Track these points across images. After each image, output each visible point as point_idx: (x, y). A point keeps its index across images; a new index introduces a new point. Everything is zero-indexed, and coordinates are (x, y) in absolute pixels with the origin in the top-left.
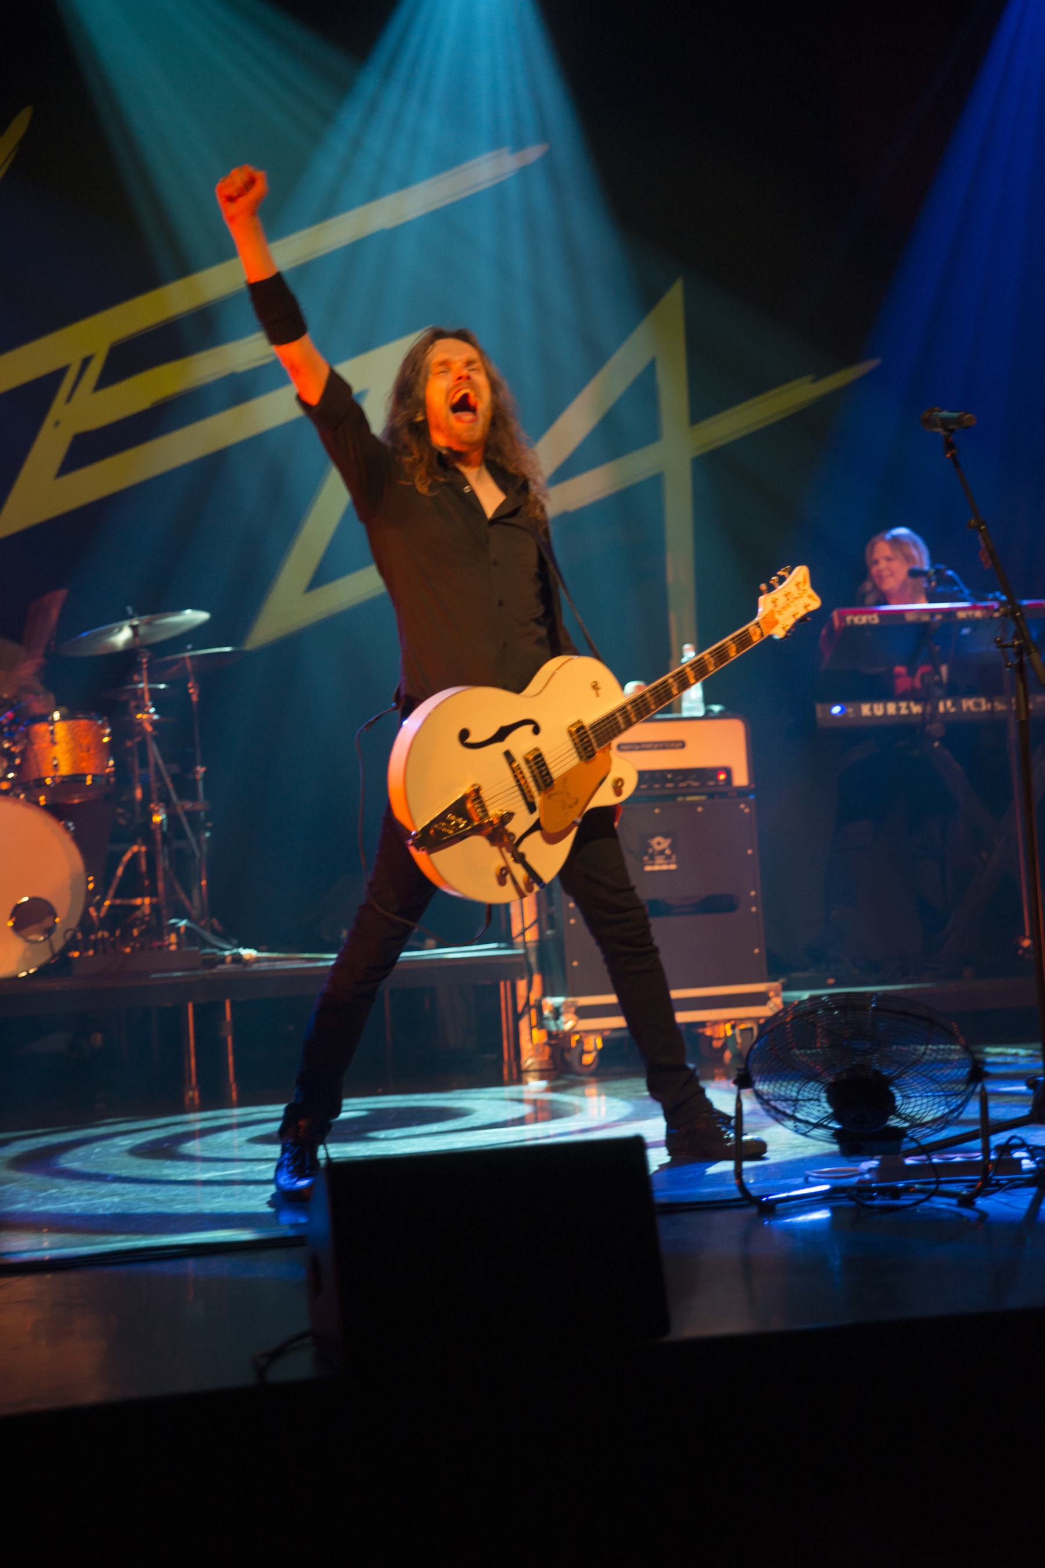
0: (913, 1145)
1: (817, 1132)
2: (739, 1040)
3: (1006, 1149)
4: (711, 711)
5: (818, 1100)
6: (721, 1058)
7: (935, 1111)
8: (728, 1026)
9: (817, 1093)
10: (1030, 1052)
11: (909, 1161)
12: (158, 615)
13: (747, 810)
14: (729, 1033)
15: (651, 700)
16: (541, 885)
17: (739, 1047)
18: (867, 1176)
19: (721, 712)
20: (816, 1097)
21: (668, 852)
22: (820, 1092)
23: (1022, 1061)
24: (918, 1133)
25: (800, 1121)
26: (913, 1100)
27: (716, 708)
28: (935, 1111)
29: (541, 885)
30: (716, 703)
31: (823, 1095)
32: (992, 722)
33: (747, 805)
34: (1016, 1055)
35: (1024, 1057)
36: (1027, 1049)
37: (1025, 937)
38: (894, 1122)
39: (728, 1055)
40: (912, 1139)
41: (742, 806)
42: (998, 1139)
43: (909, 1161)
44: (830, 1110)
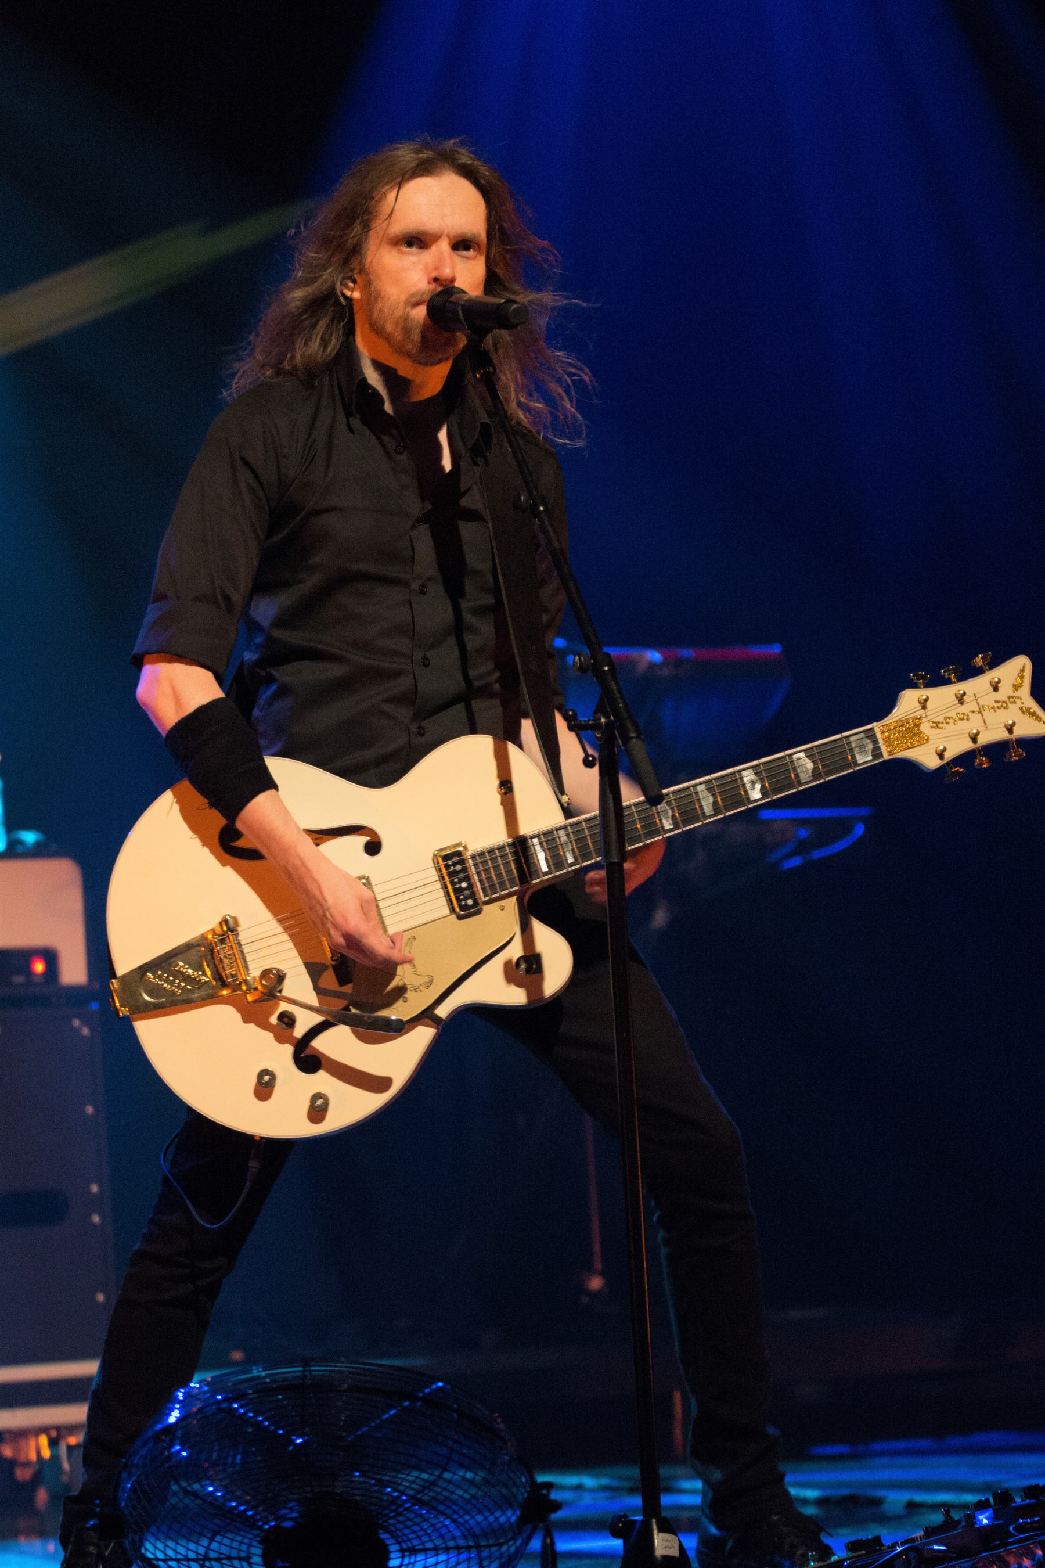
2: (66, 1466)
4: (21, 842)
5: (247, 1559)
6: (30, 1500)
8: (44, 1440)
9: (244, 1547)
10: (605, 1481)
12: (478, 299)
13: (85, 1031)
14: (46, 1453)
16: (852, 765)
17: (65, 1478)
19: (37, 844)
20: (243, 1555)
22: (250, 1545)
23: (587, 1499)
26: (420, 1557)
27: (29, 837)
29: (852, 765)
30: (27, 827)
32: (719, 804)
33: (86, 1020)
34: (579, 1487)
35: (592, 1490)
36: (596, 1476)
37: (591, 1271)
39: (42, 1496)
41: (76, 1023)
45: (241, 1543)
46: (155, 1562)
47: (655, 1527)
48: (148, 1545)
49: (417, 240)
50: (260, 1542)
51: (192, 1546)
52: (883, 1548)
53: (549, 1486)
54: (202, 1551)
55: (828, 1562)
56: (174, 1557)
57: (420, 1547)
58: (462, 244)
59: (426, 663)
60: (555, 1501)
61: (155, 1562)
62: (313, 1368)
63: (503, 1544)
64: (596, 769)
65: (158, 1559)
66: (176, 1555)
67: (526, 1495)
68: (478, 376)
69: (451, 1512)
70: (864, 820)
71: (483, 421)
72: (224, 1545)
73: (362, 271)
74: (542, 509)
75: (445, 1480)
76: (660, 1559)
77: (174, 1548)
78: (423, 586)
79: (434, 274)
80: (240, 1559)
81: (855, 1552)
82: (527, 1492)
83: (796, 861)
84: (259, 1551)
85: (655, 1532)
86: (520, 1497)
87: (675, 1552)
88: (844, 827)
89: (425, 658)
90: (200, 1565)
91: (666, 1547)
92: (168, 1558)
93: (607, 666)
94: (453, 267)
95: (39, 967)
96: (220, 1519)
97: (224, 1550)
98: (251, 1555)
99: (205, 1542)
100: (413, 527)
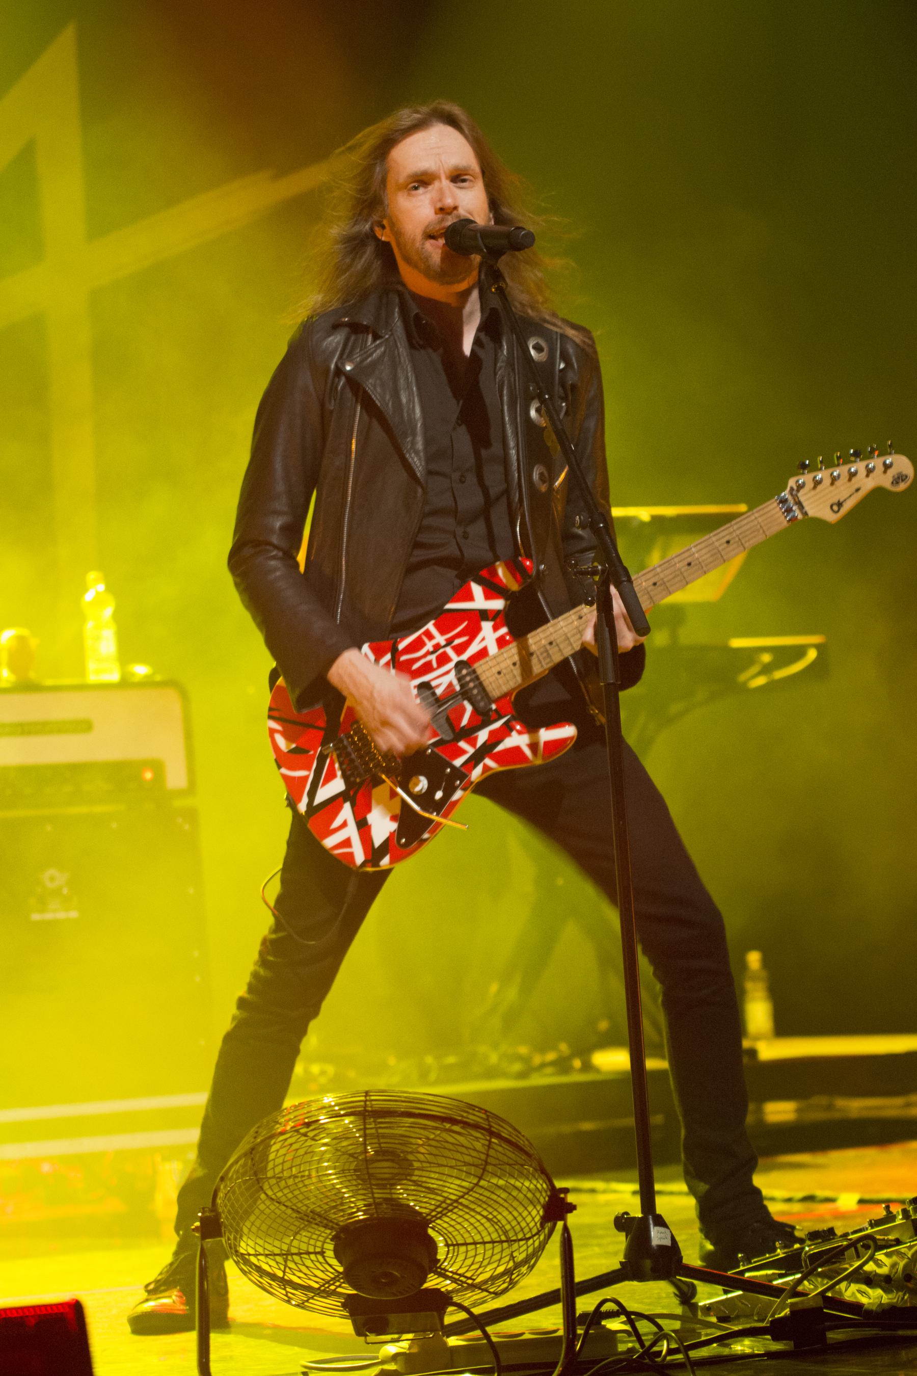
0: (463, 1315)
1: (319, 1302)
3: (598, 1315)
7: (495, 1265)
11: (453, 1341)
15: (436, 697)
18: (392, 1367)
20: (318, 1250)
21: (65, 891)
24: (467, 1298)
25: (296, 1286)
28: (495, 1265)
31: (330, 1247)
38: (433, 1282)
40: (461, 1307)
42: (585, 1304)
43: (453, 1341)
44: (341, 1269)
45: (317, 1240)
46: (247, 1257)
47: (651, 1222)
48: (243, 1244)
49: (422, 180)
50: (332, 1240)
51: (277, 1243)
52: (836, 1237)
53: (566, 1191)
54: (285, 1247)
55: (791, 1249)
56: (262, 1253)
57: (514, 1238)
58: (458, 177)
59: (465, 536)
60: (570, 1204)
61: (247, 1257)
62: (373, 1098)
63: (529, 1238)
64: (595, 606)
65: (249, 1255)
66: (264, 1251)
67: (547, 1199)
68: (493, 290)
69: (493, 1213)
70: (818, 647)
71: (492, 307)
72: (303, 1242)
73: (384, 216)
74: (547, 397)
75: (482, 1187)
76: (655, 1248)
77: (253, 1247)
78: (462, 476)
79: (439, 205)
80: (316, 1253)
81: (813, 1241)
82: (548, 1196)
83: (761, 681)
84: (331, 1247)
85: (652, 1226)
86: (542, 1200)
87: (668, 1242)
88: (798, 652)
89: (465, 532)
90: (284, 1258)
91: (661, 1238)
92: (257, 1253)
93: (602, 523)
94: (454, 197)
95: (148, 775)
96: (299, 1222)
97: (304, 1247)
98: (324, 1250)
99: (287, 1240)
100: (454, 429)
